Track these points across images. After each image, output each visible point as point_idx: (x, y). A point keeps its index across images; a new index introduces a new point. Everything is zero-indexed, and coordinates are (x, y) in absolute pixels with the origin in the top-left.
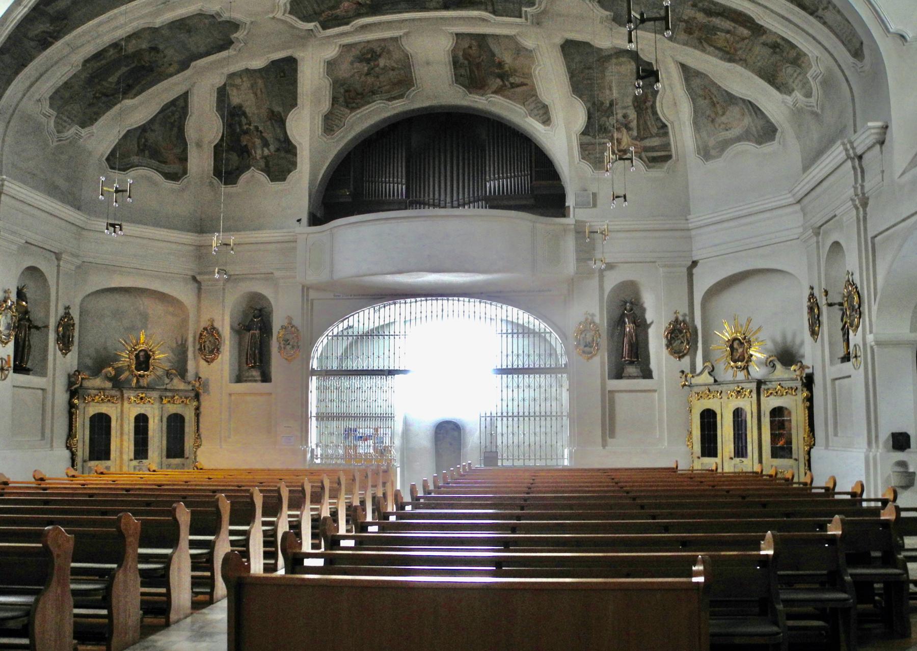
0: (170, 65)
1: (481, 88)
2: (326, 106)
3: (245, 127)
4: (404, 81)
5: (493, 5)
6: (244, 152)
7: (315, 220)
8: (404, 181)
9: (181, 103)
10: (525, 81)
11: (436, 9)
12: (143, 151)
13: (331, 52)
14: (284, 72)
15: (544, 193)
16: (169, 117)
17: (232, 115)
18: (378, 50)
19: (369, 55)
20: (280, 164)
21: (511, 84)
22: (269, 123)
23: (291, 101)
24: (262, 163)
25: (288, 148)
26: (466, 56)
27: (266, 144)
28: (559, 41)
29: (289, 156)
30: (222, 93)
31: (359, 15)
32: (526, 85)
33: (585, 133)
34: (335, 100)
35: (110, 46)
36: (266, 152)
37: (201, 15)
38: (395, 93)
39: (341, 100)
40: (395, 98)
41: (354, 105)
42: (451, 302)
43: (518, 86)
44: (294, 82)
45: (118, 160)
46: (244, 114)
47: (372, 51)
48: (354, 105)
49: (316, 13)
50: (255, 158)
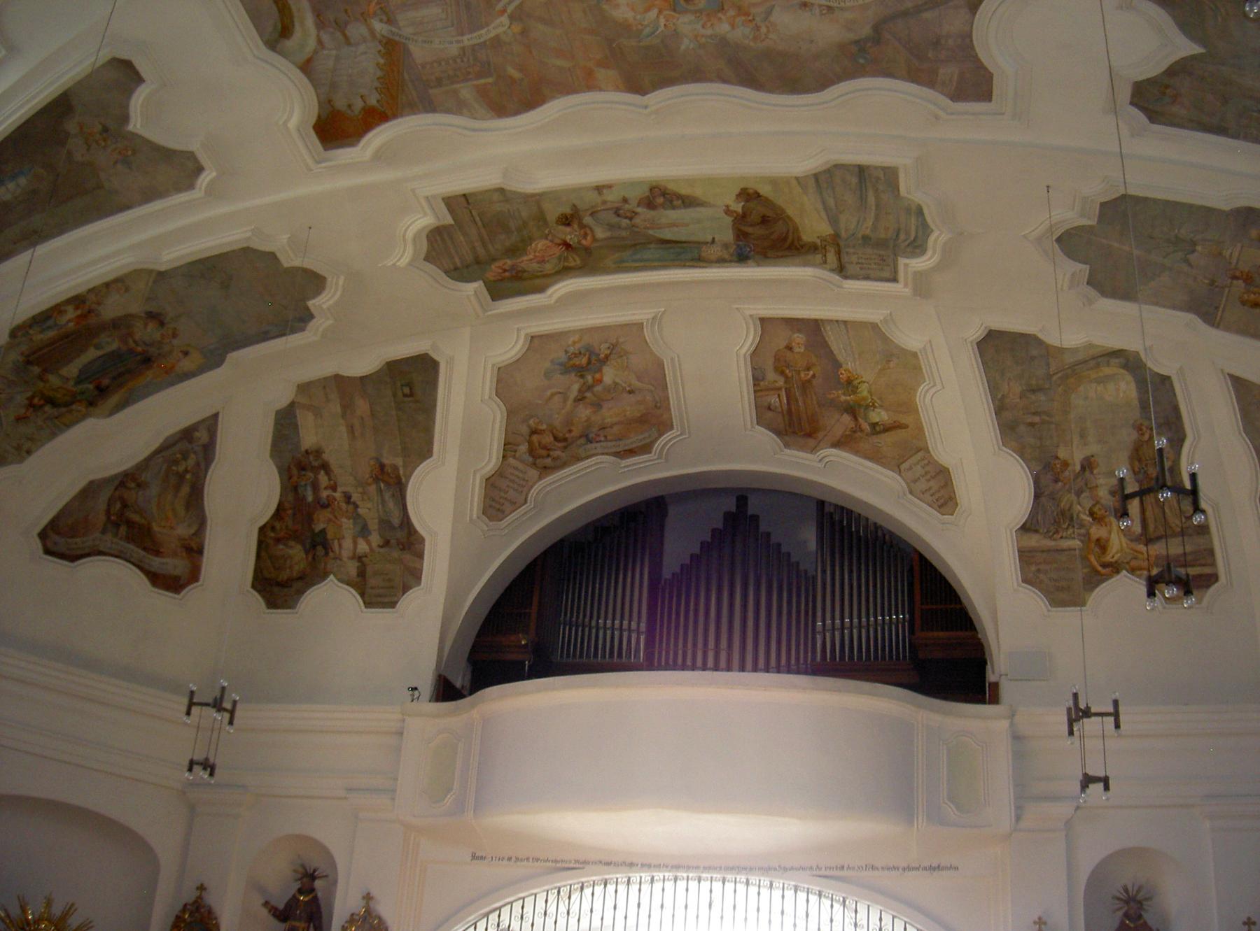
0: (186, 354)
1: (809, 435)
2: (490, 460)
3: (324, 494)
4: (653, 420)
5: (839, 253)
6: (319, 545)
7: (446, 691)
8: (643, 626)
9: (202, 436)
10: (904, 419)
11: (721, 261)
12: (117, 525)
13: (508, 348)
14: (412, 382)
15: (937, 649)
16: (176, 462)
17: (299, 468)
18: (604, 350)
19: (586, 361)
20: (389, 569)
21: (874, 425)
22: (372, 489)
23: (420, 447)
24: (352, 568)
25: (406, 541)
26: (781, 366)
27: (364, 531)
28: (976, 333)
29: (407, 556)
30: (286, 421)
31: (565, 271)
32: (905, 427)
33: (1025, 528)
34: (509, 448)
35: (69, 301)
36: (363, 547)
37: (247, 253)
38: (633, 441)
39: (523, 448)
40: (631, 452)
41: (548, 461)
42: (729, 886)
43: (887, 429)
44: (429, 409)
45: (64, 538)
46: (325, 467)
47: (590, 351)
48: (548, 461)
49: (478, 262)
50: (338, 558)
